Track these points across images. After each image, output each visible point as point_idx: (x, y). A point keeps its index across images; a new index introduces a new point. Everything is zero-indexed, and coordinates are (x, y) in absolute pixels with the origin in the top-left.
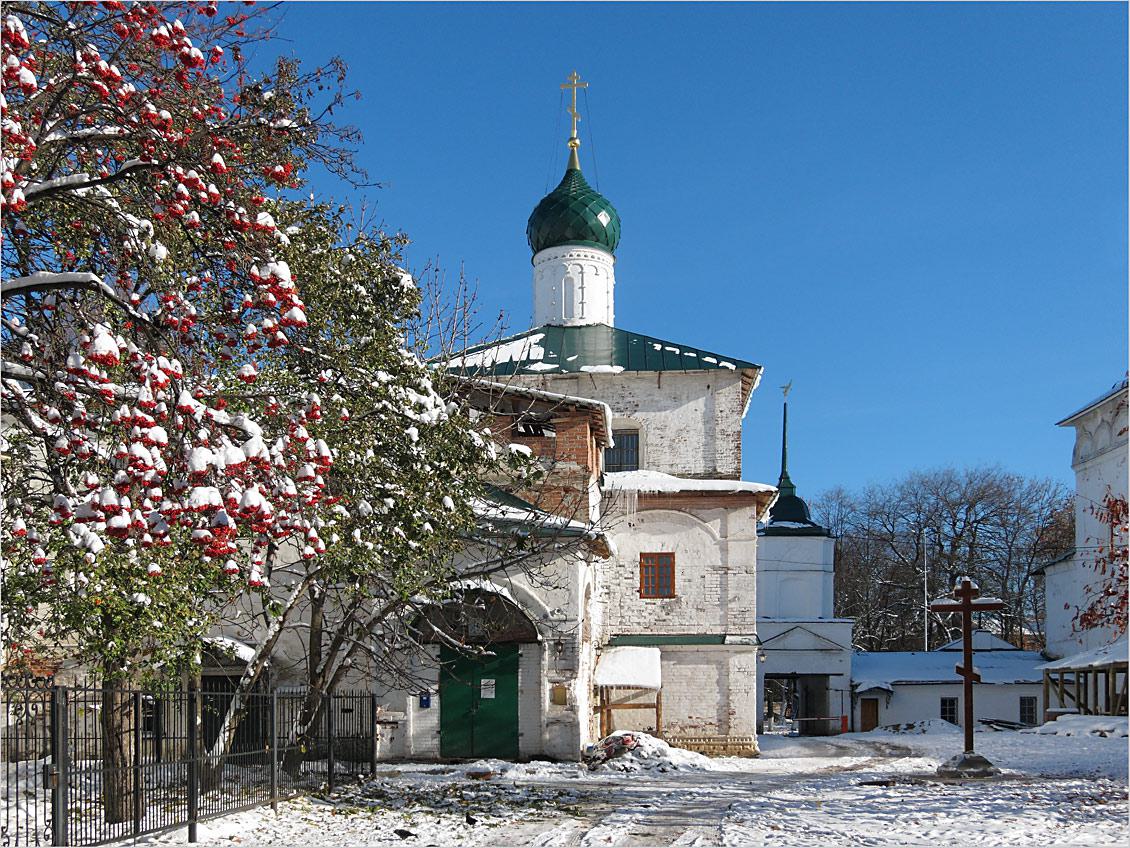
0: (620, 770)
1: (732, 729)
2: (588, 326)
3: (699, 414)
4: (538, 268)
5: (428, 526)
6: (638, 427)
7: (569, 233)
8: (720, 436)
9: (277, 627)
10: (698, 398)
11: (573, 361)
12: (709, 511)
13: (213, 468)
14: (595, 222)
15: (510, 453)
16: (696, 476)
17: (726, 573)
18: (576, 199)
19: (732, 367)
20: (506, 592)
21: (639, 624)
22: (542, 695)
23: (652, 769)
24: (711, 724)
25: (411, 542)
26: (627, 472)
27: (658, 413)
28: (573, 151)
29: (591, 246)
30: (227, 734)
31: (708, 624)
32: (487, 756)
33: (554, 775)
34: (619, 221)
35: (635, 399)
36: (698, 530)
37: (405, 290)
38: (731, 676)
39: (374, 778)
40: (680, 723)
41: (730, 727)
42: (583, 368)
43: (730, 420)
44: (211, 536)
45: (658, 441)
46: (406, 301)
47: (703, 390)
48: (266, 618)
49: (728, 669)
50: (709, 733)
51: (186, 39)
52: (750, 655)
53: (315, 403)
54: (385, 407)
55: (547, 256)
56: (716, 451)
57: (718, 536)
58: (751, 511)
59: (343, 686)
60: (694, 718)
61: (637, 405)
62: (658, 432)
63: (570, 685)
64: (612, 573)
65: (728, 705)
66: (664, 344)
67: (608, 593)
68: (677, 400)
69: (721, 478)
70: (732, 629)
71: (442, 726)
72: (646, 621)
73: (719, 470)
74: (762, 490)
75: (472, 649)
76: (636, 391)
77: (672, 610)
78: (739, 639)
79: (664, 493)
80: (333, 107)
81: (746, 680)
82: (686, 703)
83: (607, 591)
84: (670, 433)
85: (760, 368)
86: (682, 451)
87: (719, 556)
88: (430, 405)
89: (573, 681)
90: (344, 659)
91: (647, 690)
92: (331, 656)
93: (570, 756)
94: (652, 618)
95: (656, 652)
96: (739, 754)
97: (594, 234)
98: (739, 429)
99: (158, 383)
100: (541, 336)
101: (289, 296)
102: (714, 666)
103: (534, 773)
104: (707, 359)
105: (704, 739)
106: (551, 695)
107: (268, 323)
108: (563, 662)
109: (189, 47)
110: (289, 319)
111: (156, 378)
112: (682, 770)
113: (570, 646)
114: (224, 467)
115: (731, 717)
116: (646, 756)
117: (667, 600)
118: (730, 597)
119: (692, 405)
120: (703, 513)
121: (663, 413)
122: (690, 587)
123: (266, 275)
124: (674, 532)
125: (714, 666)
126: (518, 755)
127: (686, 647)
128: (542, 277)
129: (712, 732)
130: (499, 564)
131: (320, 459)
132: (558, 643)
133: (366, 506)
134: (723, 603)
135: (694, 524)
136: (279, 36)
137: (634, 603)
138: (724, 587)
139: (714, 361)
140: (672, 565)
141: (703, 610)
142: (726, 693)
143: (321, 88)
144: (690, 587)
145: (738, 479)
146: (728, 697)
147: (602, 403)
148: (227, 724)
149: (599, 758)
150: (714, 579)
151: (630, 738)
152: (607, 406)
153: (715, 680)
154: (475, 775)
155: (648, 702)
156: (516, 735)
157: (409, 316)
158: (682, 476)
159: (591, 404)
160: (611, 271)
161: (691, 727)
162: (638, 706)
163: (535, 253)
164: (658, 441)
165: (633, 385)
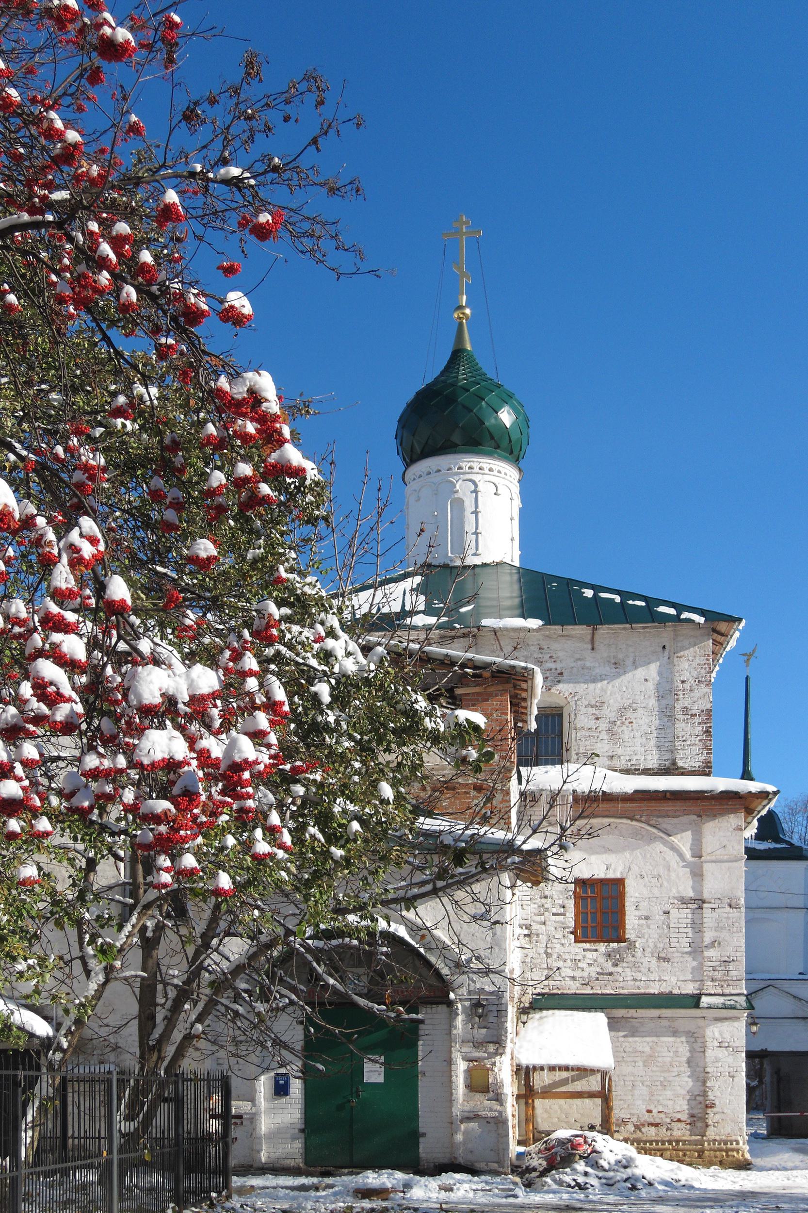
0: (569, 1186)
1: (711, 1128)
2: (485, 565)
3: (651, 686)
4: (413, 486)
5: (355, 826)
6: (562, 704)
7: (456, 438)
8: (682, 717)
9: (101, 978)
10: (649, 663)
11: (468, 611)
12: (675, 820)
13: (170, 701)
14: (493, 421)
15: (457, 724)
16: (646, 772)
17: (701, 908)
18: (468, 390)
19: (700, 619)
20: (402, 931)
21: (573, 978)
22: (454, 1078)
23: (617, 1185)
24: (679, 1120)
25: (333, 849)
26: (549, 767)
27: (592, 686)
28: (461, 324)
29: (489, 454)
30: (30, 1133)
31: (674, 980)
32: (377, 1166)
33: (480, 1193)
34: (527, 420)
35: (559, 665)
36: (659, 846)
37: (308, 482)
38: (709, 1053)
39: (229, 1197)
40: (634, 1119)
41: (707, 1126)
42: (485, 622)
43: (696, 694)
44: (174, 810)
45: (592, 723)
46: (310, 498)
47: (654, 652)
48: (85, 964)
49: (704, 1042)
50: (677, 1134)
51: (107, 15)
52: (736, 1024)
53: (270, 615)
54: (278, 653)
55: (425, 470)
56: (675, 737)
57: (688, 855)
58: (735, 820)
59: (189, 1064)
60: (655, 1111)
61: (561, 674)
62: (592, 711)
63: (494, 1064)
64: (533, 908)
65: (704, 1094)
66: (596, 588)
67: (528, 936)
68: (618, 666)
69: (682, 774)
70: (710, 987)
71: (306, 1123)
72: (585, 974)
73: (680, 764)
74: (753, 790)
75: (387, 1011)
76: (560, 654)
77: (622, 960)
78: (719, 1000)
79: (611, 794)
80: (319, 139)
81: (730, 1060)
82: (642, 1091)
83: (526, 932)
84: (609, 713)
85: (740, 620)
86: (626, 737)
87: (691, 883)
88: (340, 653)
89: (498, 1058)
90: (192, 1025)
91: (583, 1072)
92: (171, 1022)
93: (495, 1166)
94: (593, 971)
95: (599, 1019)
96: (722, 1164)
97: (492, 438)
98: (708, 706)
99: (82, 558)
100: (418, 579)
101: (278, 425)
102: (683, 1039)
103: (451, 1190)
104: (662, 609)
105: (670, 1142)
106: (466, 1079)
107: (245, 469)
108: (484, 1031)
109: (110, 26)
110: (277, 463)
111: (77, 550)
112: (660, 1187)
113: (494, 1008)
114: (187, 699)
115: (709, 1111)
116: (606, 1166)
117: (615, 945)
118: (707, 940)
119: (640, 673)
120: (667, 823)
121: (599, 685)
122: (648, 927)
123: (239, 391)
124: (623, 849)
125: (683, 1039)
126: (419, 1165)
127: (642, 1013)
128: (418, 499)
129: (681, 1132)
130: (429, 887)
131: (271, 706)
132: (477, 1004)
133: (265, 796)
134: (696, 950)
135: (652, 839)
136: (224, 33)
137: (567, 949)
138: (697, 927)
139: (672, 611)
140: (620, 897)
141: (666, 960)
142: (702, 1078)
143: (287, 119)
144: (648, 927)
145: (708, 775)
146: (704, 1082)
147: (530, 666)
148: (29, 1118)
149: (534, 1169)
150: (682, 916)
151: (581, 1140)
152: (537, 669)
153: (685, 1059)
154: (367, 1193)
155: (587, 1089)
156: (415, 1136)
157: (312, 521)
158: (627, 771)
159: (513, 667)
160: (516, 489)
161: (652, 1125)
162: (579, 1095)
163: (408, 465)
164: (592, 723)
165: (555, 646)
